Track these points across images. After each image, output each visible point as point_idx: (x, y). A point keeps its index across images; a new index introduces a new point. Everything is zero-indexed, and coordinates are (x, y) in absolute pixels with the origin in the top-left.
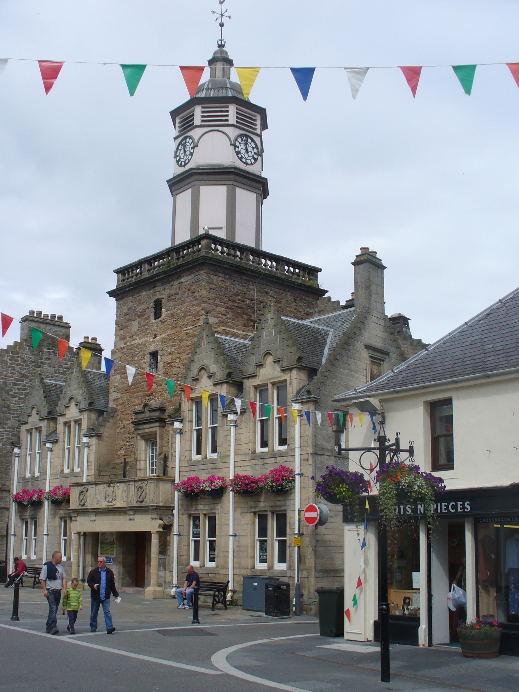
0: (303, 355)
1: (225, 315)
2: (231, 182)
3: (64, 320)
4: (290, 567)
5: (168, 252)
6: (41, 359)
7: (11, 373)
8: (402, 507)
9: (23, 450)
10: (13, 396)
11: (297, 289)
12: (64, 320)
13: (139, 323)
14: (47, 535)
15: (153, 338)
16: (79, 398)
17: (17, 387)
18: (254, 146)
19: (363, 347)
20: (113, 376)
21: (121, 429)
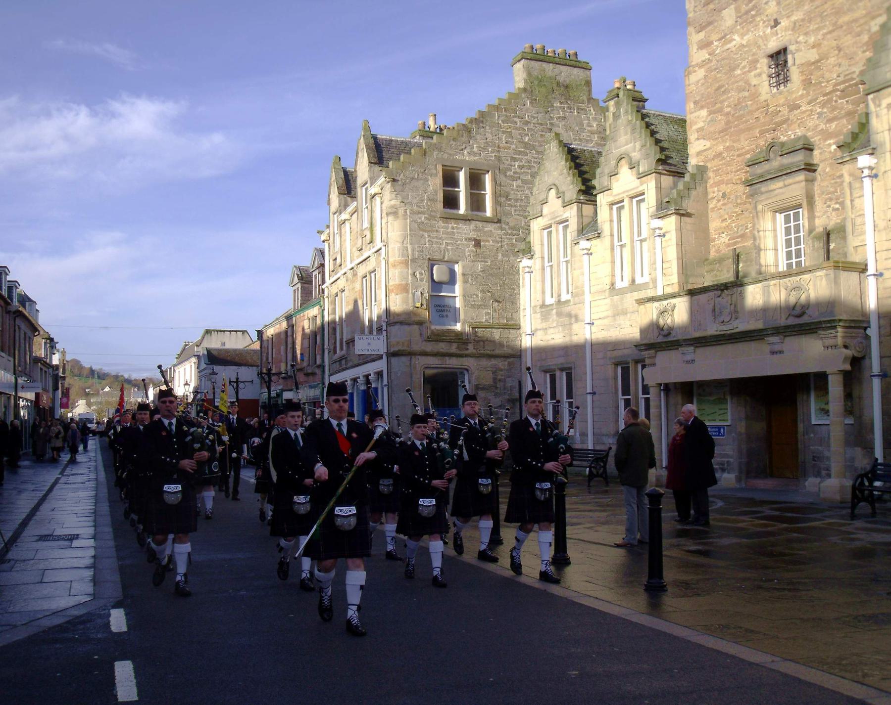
10: (514, 179)
13: (737, 10)
14: (594, 393)
15: (772, 27)
17: (517, 164)
20: (692, 113)
21: (719, 201)
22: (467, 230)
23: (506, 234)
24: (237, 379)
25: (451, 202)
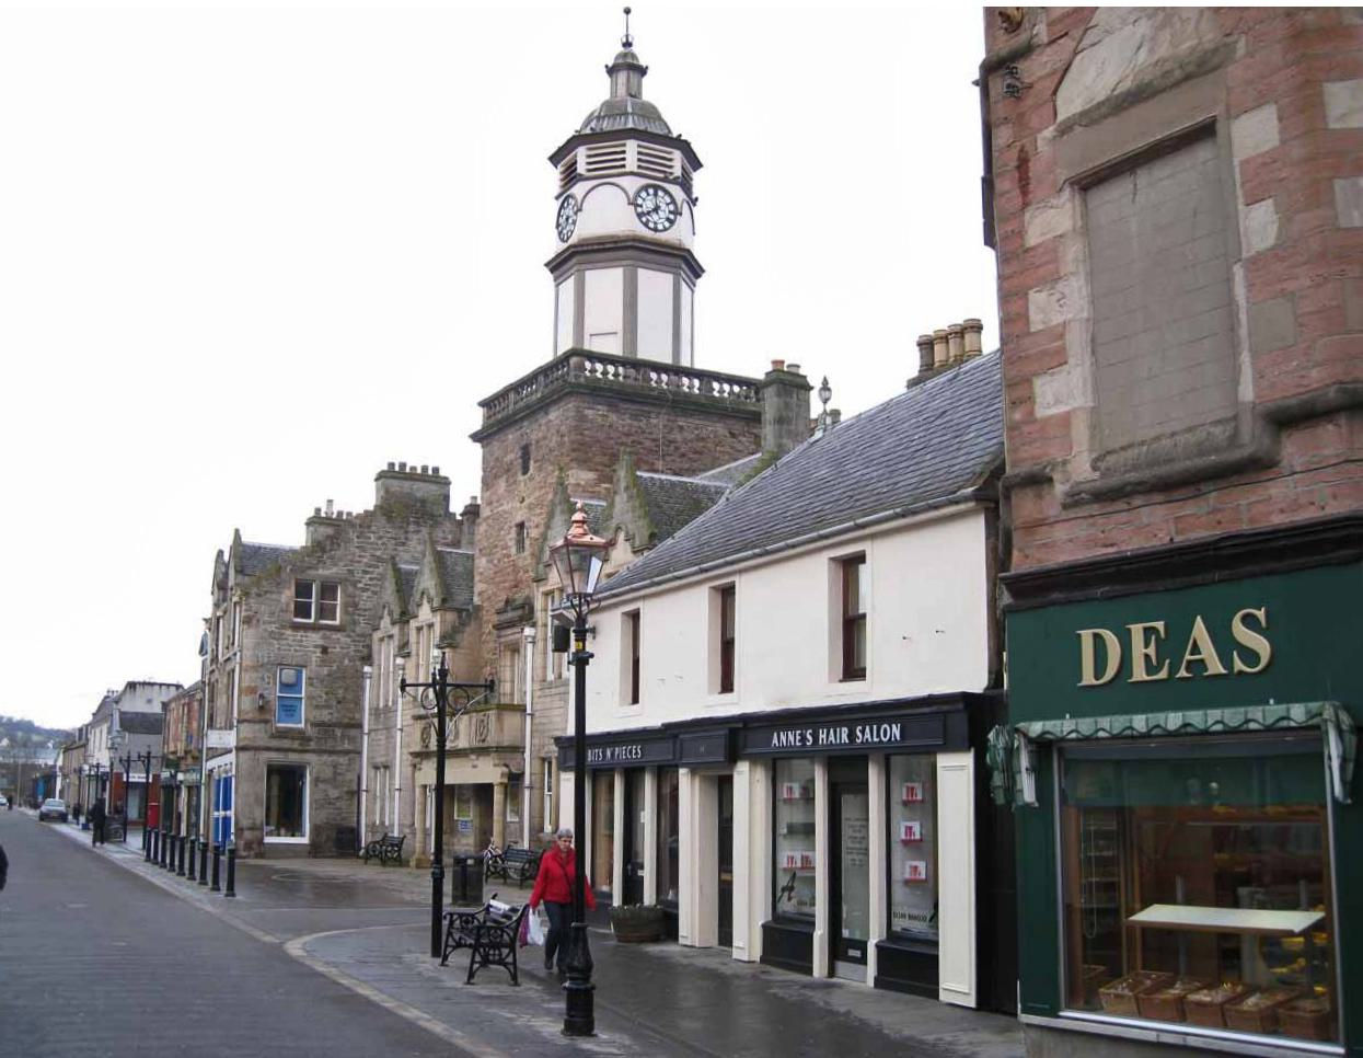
0: (656, 531)
1: (609, 466)
5: (545, 371)
7: (360, 556)
8: (875, 740)
11: (735, 417)
16: (432, 592)
17: (368, 576)
18: (668, 200)
22: (315, 638)
23: (354, 641)
24: (129, 757)
25: (302, 610)
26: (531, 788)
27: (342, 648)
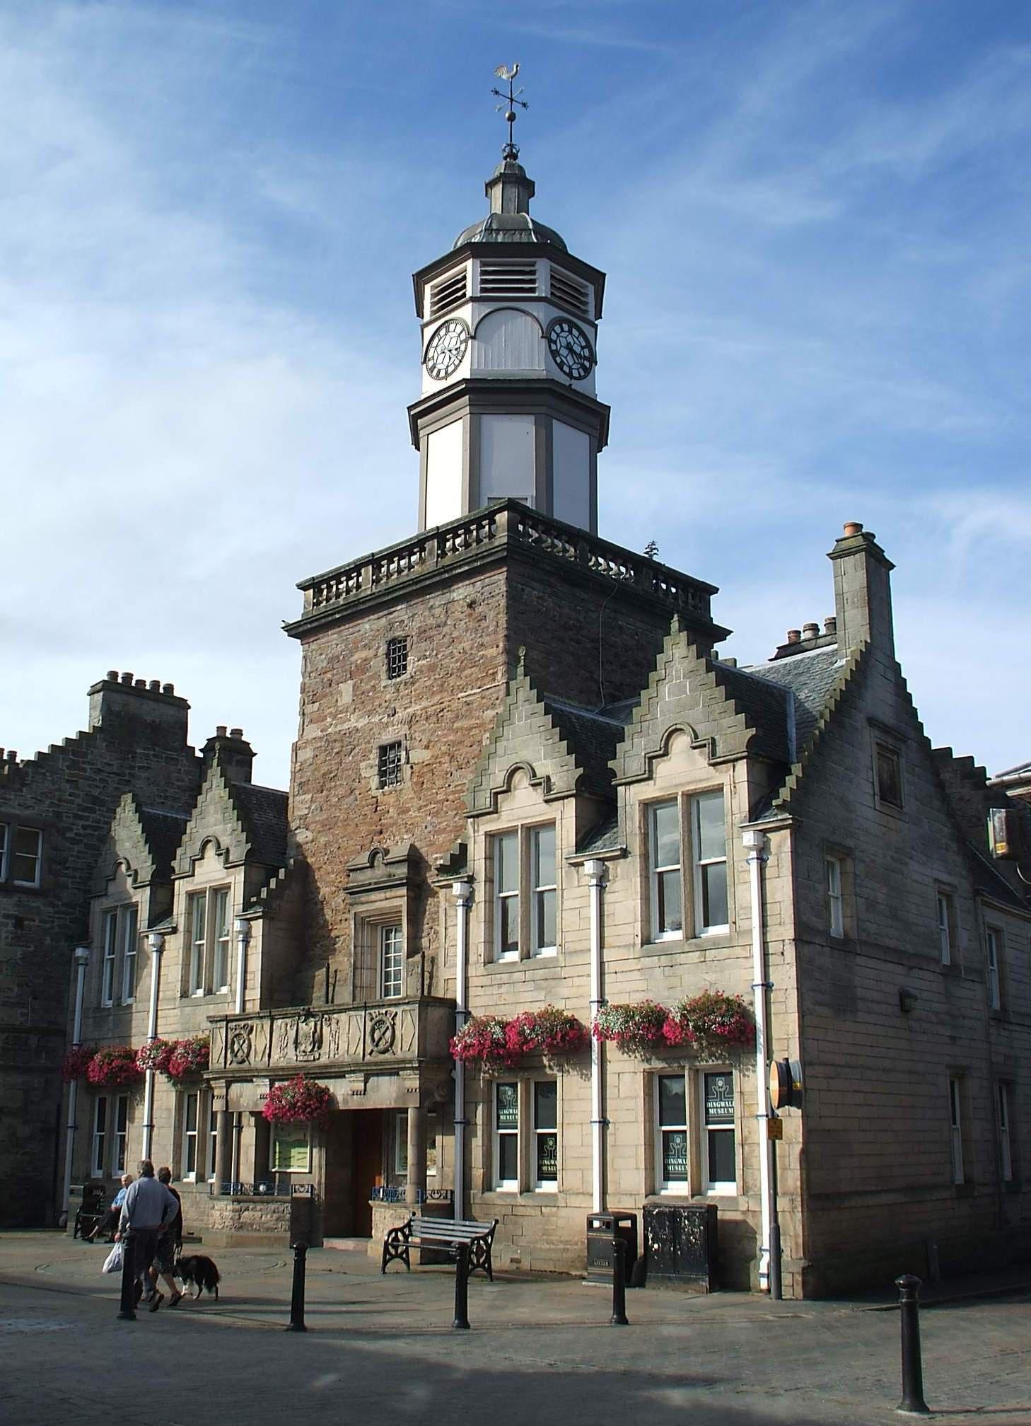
2: (543, 410)
3: (176, 694)
4: (745, 1190)
5: (419, 544)
6: (132, 767)
9: (96, 952)
10: (74, 841)
12: (176, 694)
17: (81, 823)
19: (865, 724)
26: (75, 1128)
27: (41, 921)
